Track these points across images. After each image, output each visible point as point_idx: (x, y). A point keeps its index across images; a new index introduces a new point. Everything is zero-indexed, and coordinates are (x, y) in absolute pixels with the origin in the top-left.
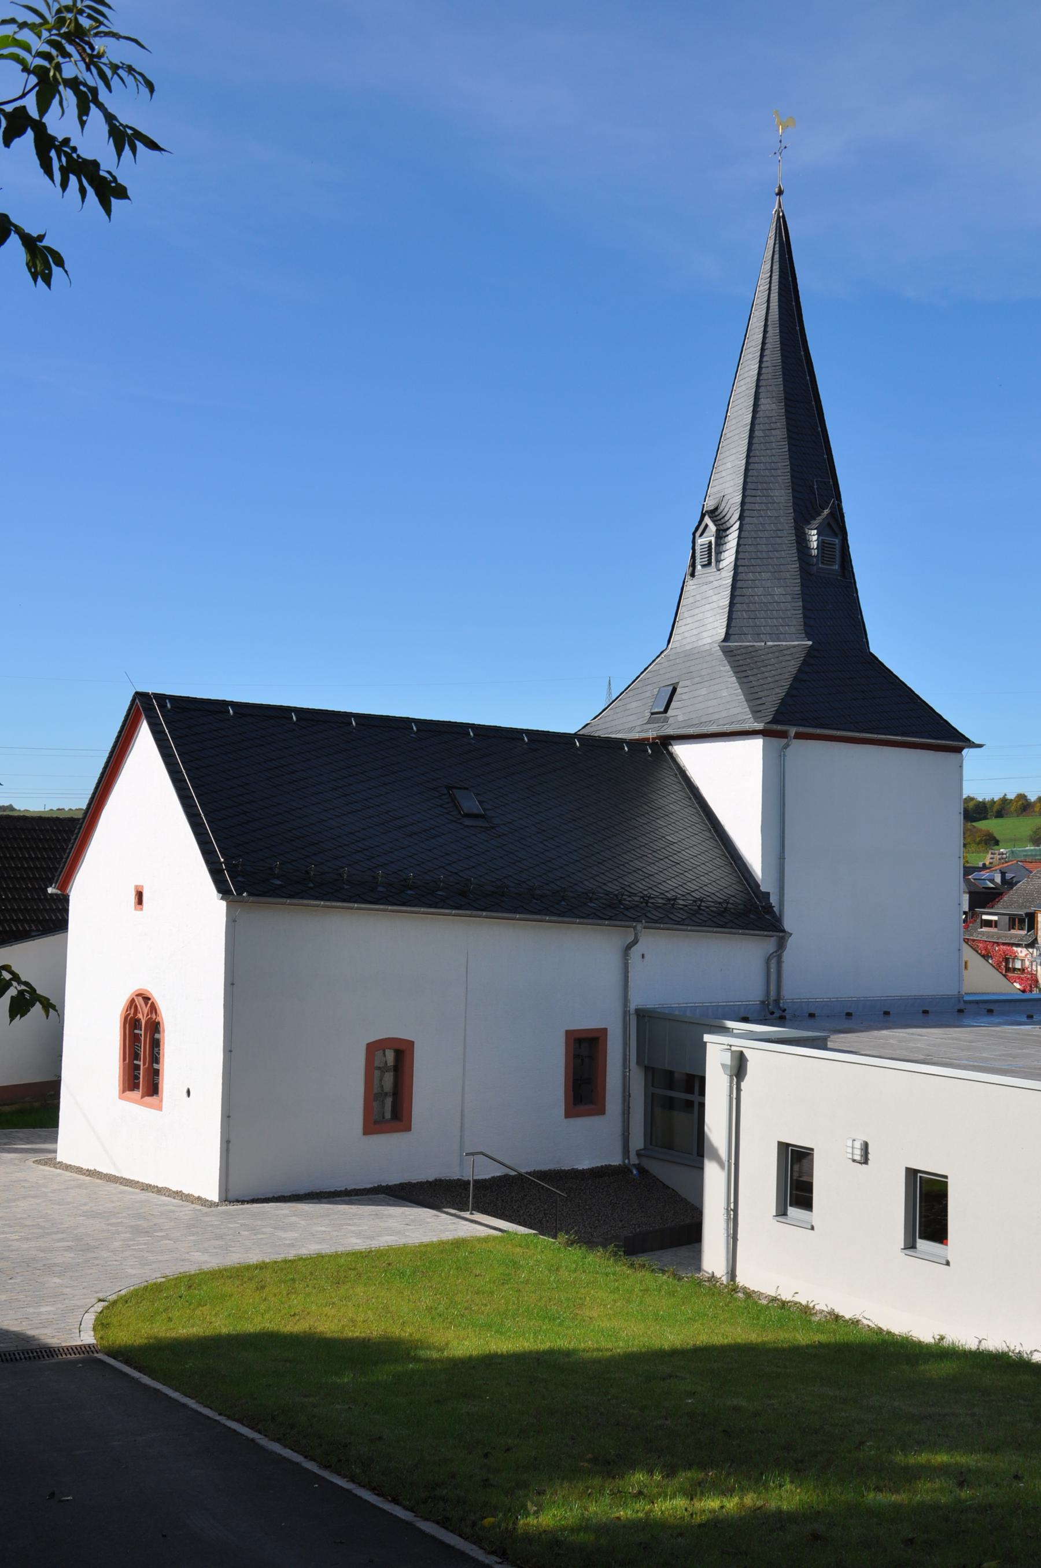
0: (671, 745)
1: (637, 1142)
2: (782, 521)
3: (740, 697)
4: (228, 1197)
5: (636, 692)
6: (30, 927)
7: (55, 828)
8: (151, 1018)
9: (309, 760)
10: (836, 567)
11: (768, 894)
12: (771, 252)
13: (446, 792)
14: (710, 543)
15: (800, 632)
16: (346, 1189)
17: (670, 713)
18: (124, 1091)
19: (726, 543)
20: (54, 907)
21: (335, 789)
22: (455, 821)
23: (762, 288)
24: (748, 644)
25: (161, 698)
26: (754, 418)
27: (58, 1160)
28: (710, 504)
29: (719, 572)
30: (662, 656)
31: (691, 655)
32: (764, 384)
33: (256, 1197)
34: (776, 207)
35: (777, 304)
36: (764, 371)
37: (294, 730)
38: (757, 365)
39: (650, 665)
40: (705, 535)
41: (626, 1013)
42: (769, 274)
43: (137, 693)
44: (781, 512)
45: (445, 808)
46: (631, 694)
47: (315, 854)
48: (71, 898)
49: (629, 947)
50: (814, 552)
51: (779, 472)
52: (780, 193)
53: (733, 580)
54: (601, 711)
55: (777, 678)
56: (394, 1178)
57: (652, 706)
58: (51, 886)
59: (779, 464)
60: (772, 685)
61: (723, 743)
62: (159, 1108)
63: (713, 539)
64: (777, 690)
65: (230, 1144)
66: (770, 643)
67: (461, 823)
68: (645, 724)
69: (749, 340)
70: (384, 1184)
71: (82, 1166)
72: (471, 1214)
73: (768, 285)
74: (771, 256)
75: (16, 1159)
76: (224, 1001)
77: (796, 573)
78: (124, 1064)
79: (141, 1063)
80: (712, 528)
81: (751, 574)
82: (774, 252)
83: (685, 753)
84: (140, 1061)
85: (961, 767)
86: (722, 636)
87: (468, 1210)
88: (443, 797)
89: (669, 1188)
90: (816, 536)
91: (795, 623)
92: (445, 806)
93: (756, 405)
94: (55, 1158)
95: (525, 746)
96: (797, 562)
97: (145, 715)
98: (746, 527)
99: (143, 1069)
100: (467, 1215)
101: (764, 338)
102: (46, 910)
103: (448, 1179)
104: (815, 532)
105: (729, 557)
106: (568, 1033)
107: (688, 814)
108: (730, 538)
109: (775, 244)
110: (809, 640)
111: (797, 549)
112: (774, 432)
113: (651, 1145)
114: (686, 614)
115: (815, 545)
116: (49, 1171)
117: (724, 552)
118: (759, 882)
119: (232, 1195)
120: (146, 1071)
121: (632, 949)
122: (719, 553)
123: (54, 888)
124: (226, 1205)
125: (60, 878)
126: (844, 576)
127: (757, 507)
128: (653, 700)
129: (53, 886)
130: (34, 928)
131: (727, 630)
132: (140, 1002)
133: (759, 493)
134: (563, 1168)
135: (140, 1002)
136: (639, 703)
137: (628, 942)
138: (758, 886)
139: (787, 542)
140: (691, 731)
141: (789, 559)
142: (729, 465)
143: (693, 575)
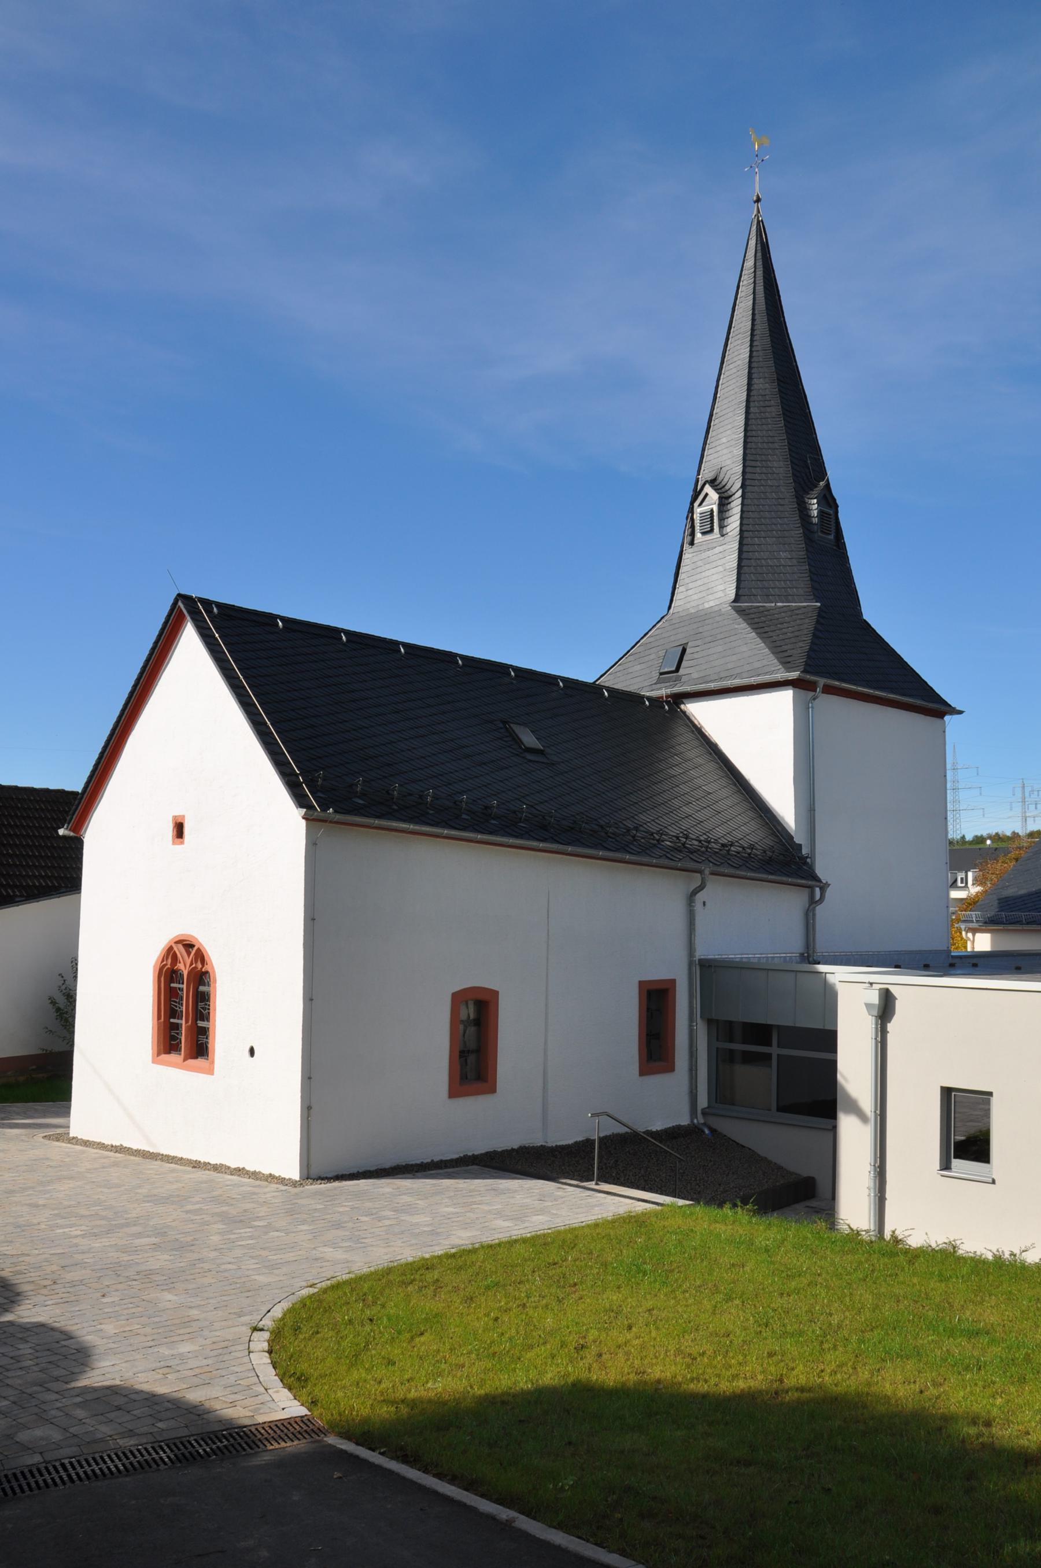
0: (683, 703)
1: (703, 1102)
2: (783, 490)
3: (765, 651)
4: (311, 1173)
5: (637, 656)
6: (14, 892)
7: (32, 798)
8: (196, 968)
9: (366, 681)
10: (832, 537)
12: (754, 250)
13: (501, 725)
14: (712, 511)
15: (808, 594)
16: (432, 1161)
17: (682, 671)
18: (159, 1054)
19: (729, 510)
20: (37, 874)
21: (398, 712)
22: (517, 755)
23: (745, 282)
24: (758, 604)
25: (207, 603)
26: (748, 396)
27: (71, 1135)
28: (706, 474)
29: (722, 538)
30: (664, 620)
31: (701, 618)
32: (756, 366)
33: (340, 1173)
34: (755, 212)
35: (763, 295)
36: (755, 354)
37: (345, 651)
38: (748, 349)
39: (650, 630)
40: (704, 504)
41: (691, 964)
42: (753, 270)
43: (179, 595)
44: (781, 481)
45: (505, 741)
46: (631, 658)
47: (392, 775)
48: (86, 841)
49: (695, 893)
50: (815, 520)
51: (776, 446)
52: (758, 200)
53: (739, 544)
54: (599, 676)
55: (797, 634)
56: (479, 1148)
57: (661, 666)
58: (63, 827)
59: (776, 438)
60: (793, 640)
61: (746, 697)
62: (210, 1071)
63: (715, 508)
64: (801, 644)
66: (779, 604)
67: (523, 757)
68: (655, 684)
69: (735, 329)
70: (470, 1154)
71: (103, 1142)
72: (597, 1184)
73: (753, 279)
74: (753, 254)
75: (21, 1135)
76: (304, 940)
77: (801, 539)
78: (158, 1023)
80: (714, 496)
81: (756, 539)
82: (756, 251)
83: (699, 711)
84: (182, 1019)
85: (944, 732)
86: (732, 596)
87: (592, 1180)
88: (501, 730)
90: (816, 505)
91: (802, 586)
92: (505, 739)
93: (750, 385)
94: (68, 1133)
95: (560, 691)
96: (801, 528)
97: (192, 618)
98: (749, 495)
100: (592, 1184)
101: (753, 325)
102: (36, 867)
103: (531, 1145)
104: (815, 501)
105: (734, 523)
106: (641, 984)
107: (711, 767)
108: (733, 505)
109: (756, 244)
110: (816, 602)
111: (800, 516)
112: (768, 409)
113: (716, 1102)
114: (687, 581)
115: (815, 513)
116: (66, 1148)
117: (727, 518)
118: (793, 834)
119: (315, 1171)
120: (187, 1029)
121: (697, 895)
122: (722, 520)
123: (67, 829)
124: (311, 1184)
125: (74, 817)
126: (838, 546)
127: (757, 476)
128: (661, 661)
129: (65, 827)
130: (17, 893)
131: (736, 591)
132: (180, 950)
133: (759, 464)
135: (180, 950)
136: (643, 666)
137: (691, 890)
138: (792, 838)
139: (789, 510)
140: (712, 686)
142: (724, 440)
143: (692, 543)
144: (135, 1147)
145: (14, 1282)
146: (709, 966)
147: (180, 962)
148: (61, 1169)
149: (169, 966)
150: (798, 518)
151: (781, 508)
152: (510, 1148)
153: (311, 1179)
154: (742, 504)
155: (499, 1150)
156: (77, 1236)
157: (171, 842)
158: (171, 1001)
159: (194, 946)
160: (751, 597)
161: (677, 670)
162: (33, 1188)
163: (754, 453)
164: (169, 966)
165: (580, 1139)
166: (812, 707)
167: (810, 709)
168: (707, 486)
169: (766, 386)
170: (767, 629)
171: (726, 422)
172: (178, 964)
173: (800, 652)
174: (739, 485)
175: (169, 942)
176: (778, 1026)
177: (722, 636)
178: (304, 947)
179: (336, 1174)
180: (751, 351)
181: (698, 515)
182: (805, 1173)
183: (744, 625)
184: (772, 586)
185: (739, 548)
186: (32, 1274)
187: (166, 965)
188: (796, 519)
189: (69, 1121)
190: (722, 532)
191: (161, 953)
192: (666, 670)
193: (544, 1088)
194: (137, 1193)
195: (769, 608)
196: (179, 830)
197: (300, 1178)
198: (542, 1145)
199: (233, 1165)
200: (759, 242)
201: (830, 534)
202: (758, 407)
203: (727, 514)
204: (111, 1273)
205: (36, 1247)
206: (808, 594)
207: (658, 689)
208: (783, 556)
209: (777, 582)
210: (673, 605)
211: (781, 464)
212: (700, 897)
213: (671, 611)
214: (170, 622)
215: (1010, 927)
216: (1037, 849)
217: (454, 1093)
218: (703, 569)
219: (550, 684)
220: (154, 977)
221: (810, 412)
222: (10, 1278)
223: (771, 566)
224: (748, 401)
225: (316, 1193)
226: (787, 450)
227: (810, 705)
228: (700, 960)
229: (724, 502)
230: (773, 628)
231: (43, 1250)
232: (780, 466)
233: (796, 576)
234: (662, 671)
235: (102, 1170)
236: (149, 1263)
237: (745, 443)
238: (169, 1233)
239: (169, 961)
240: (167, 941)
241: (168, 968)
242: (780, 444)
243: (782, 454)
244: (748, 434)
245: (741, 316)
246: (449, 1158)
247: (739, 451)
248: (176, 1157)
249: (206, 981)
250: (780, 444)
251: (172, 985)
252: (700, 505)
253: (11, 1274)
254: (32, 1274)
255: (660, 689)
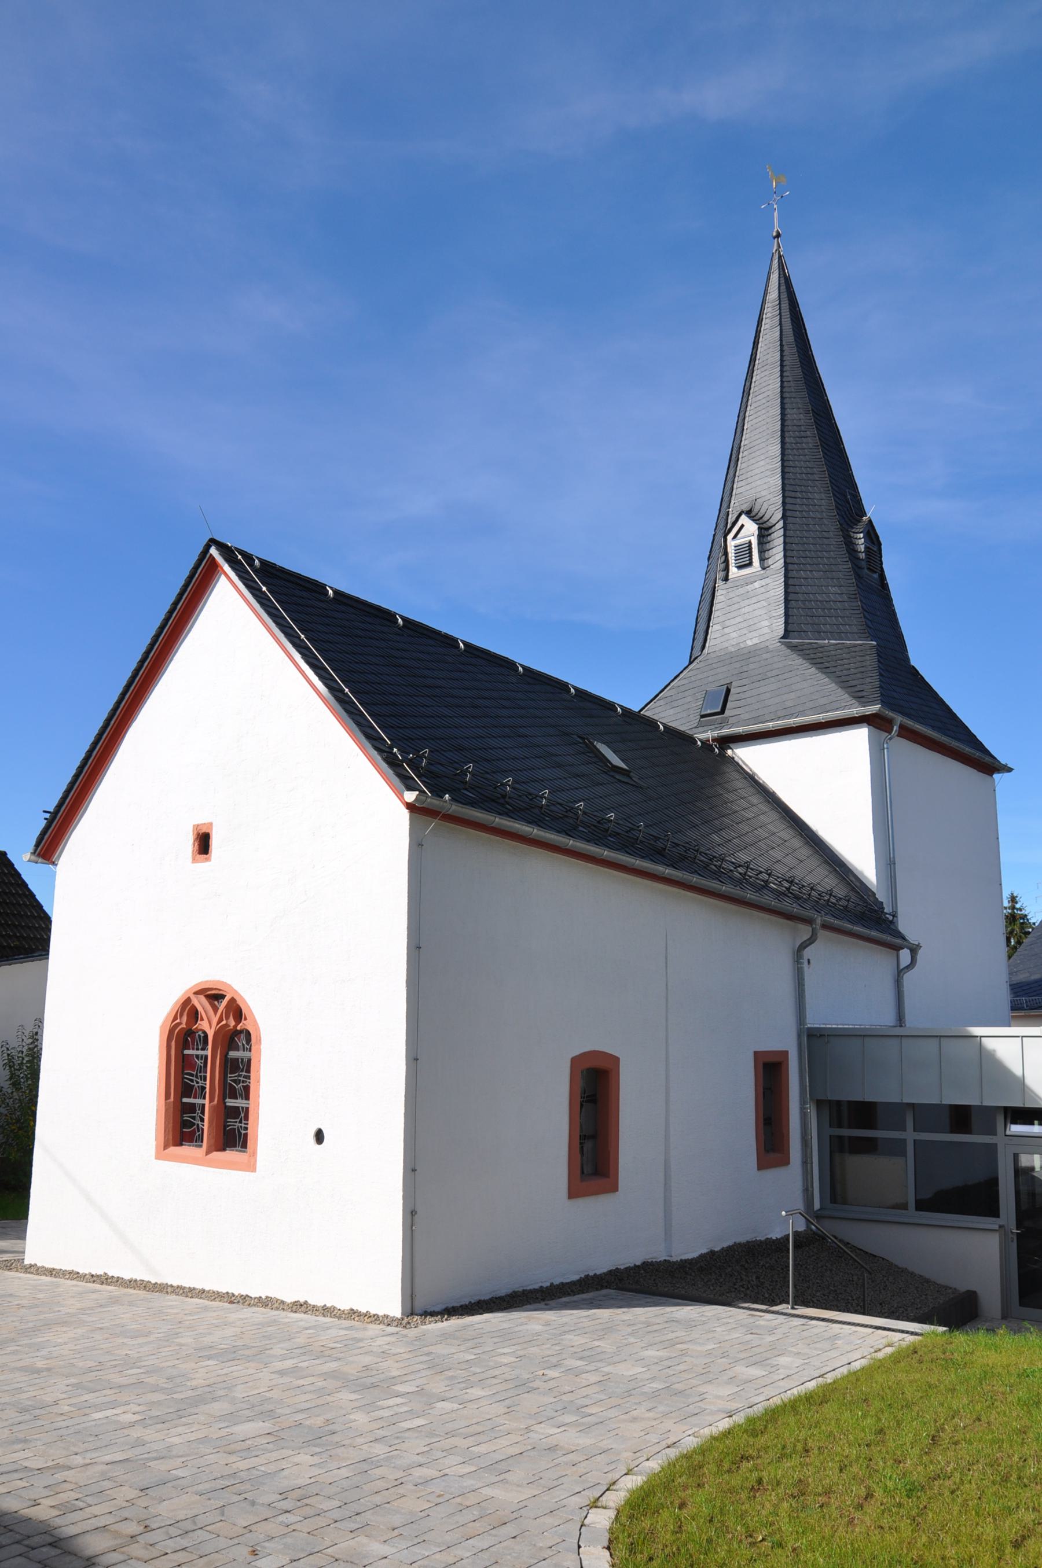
3: (829, 686)
5: (670, 699)
8: (227, 1025)
10: (876, 576)
11: (882, 902)
12: (777, 283)
14: (750, 543)
15: (862, 631)
16: (552, 1284)
17: (727, 713)
18: (166, 1147)
26: (783, 425)
27: (27, 1262)
29: (762, 572)
31: (747, 656)
34: (775, 247)
38: (779, 379)
39: (682, 672)
40: (739, 536)
42: (778, 302)
44: (824, 514)
46: (662, 702)
50: (862, 556)
52: (778, 236)
56: (601, 1266)
62: (251, 1167)
65: (416, 1217)
68: (696, 727)
69: (760, 361)
70: (591, 1274)
72: (793, 1308)
79: (207, 1102)
82: (779, 284)
83: (748, 756)
84: (204, 1098)
86: (781, 632)
89: (875, 1256)
90: (863, 540)
93: (783, 415)
96: (849, 563)
99: (210, 1107)
101: (782, 356)
104: (862, 535)
106: (756, 1054)
107: (771, 817)
108: (773, 536)
109: (779, 277)
110: (872, 640)
115: (862, 548)
118: (874, 890)
119: (419, 1306)
120: (213, 1109)
121: (806, 950)
127: (798, 507)
128: (702, 702)
132: (201, 1004)
134: (758, 1239)
135: (201, 1004)
139: (835, 543)
140: (770, 725)
141: (839, 560)
143: (726, 579)
144: (127, 1276)
145: (72, 1531)
146: (821, 1035)
147: (202, 1020)
148: (40, 1309)
149: (184, 1026)
150: (845, 552)
151: (826, 541)
152: (632, 1265)
153: (416, 1315)
154: (785, 535)
155: (622, 1267)
156: (132, 1425)
157: (191, 860)
158: (183, 1073)
159: (223, 997)
160: (801, 633)
161: (723, 711)
162: (13, 1340)
163: (793, 483)
164: (184, 1026)
165: (704, 1251)
166: (887, 748)
167: (886, 750)
168: (743, 516)
169: (799, 416)
170: (827, 665)
171: (758, 453)
172: (199, 1022)
173: (871, 687)
174: (780, 515)
175: (187, 992)
176: (913, 1106)
177: (774, 673)
178: (407, 986)
179: (444, 1307)
180: (782, 382)
181: (733, 548)
182: (963, 1287)
183: (800, 661)
184: (823, 622)
185: (784, 581)
186: (96, 1510)
187: (180, 1024)
188: (844, 552)
189: (25, 1244)
190: (764, 565)
191: (172, 1010)
192: (709, 712)
193: (665, 1185)
194: (181, 1345)
195: (823, 645)
196: (203, 843)
197: (403, 1314)
198: (665, 1260)
199: (289, 1299)
200: (781, 276)
201: (876, 572)
202: (794, 437)
203: (768, 546)
204: (236, 1498)
205: (76, 1450)
206: (862, 631)
207: (704, 732)
208: (833, 592)
209: (827, 618)
210: (707, 645)
211: (823, 496)
212: (808, 953)
213: (706, 651)
214: (197, 576)
215: (1033, 1013)
216: (1039, 934)
217: (574, 1193)
218: (742, 604)
219: (611, 710)
220: (161, 1041)
221: (844, 447)
222: (58, 1522)
223: (820, 601)
224: (783, 431)
225: (445, 1337)
226: (828, 482)
227: (885, 746)
228: (809, 1029)
229: (764, 533)
230: (834, 664)
231: (89, 1455)
232: (821, 498)
233: (848, 613)
234: (703, 713)
235: (100, 1310)
236: (285, 1473)
237: (783, 473)
238: (279, 1411)
239: (185, 1019)
240: (183, 992)
241: (183, 1028)
242: (820, 476)
243: (824, 486)
244: (785, 464)
245: (765, 348)
246: (568, 1281)
247: (777, 481)
248: (194, 1289)
249: (240, 1044)
250: (820, 476)
251: (186, 1052)
252: (735, 537)
253: (56, 1512)
254: (96, 1510)
255: (706, 731)
